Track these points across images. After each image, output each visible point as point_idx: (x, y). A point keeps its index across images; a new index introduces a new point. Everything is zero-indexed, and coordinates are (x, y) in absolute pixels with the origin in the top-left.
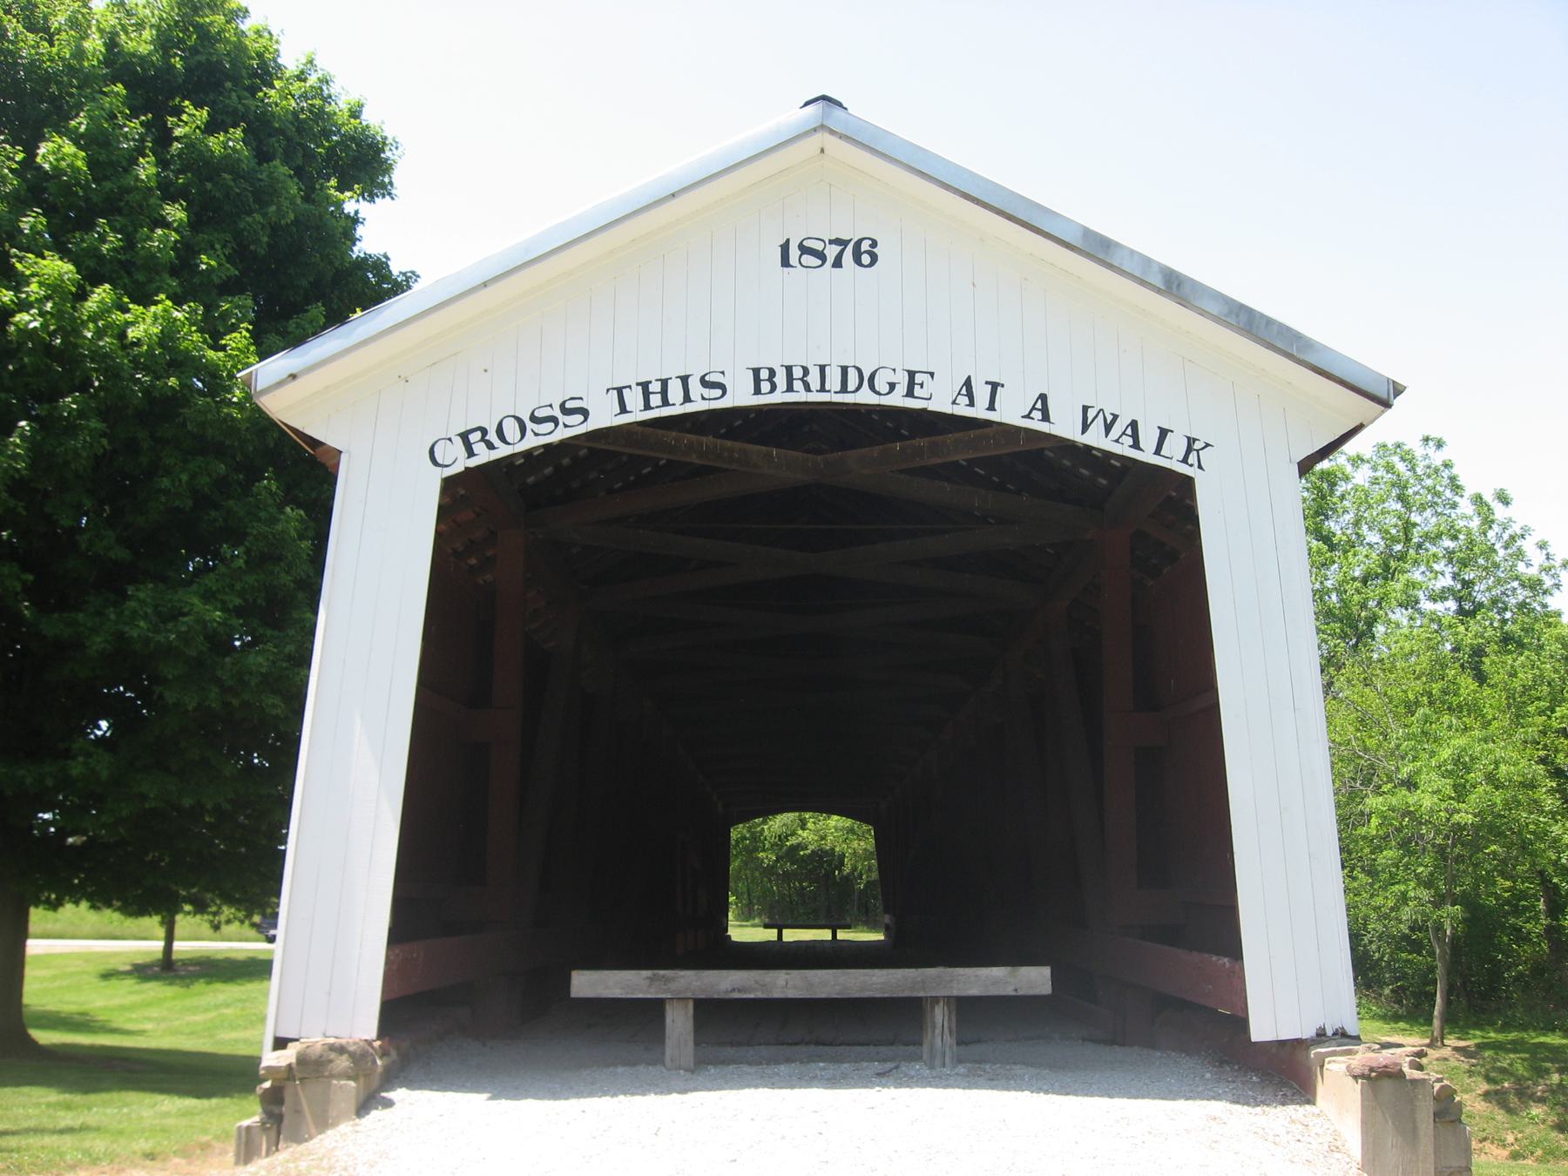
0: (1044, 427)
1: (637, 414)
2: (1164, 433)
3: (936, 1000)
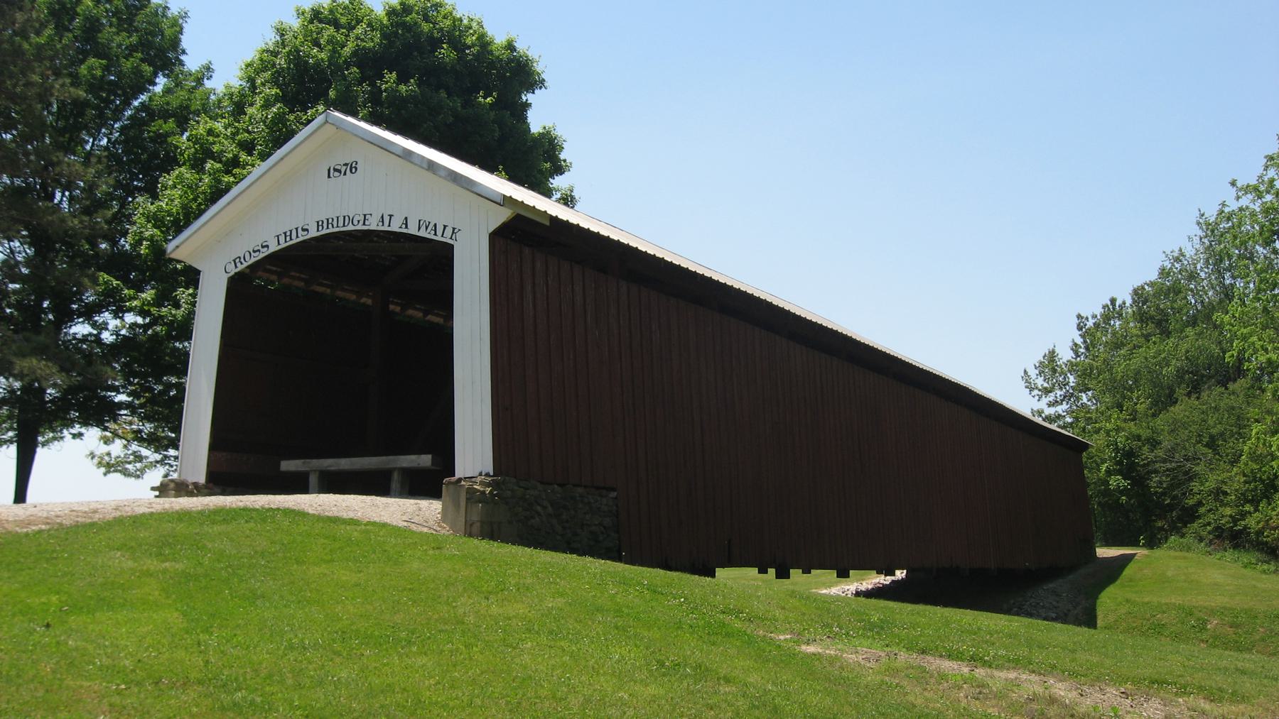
0: (405, 231)
1: (283, 245)
2: (445, 227)
3: (395, 469)
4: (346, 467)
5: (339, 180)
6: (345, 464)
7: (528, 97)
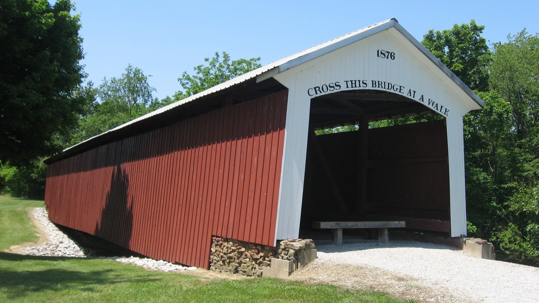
0: (421, 102)
2: (442, 107)
4: (362, 227)
5: (382, 60)
6: (361, 225)
7: (81, 62)
